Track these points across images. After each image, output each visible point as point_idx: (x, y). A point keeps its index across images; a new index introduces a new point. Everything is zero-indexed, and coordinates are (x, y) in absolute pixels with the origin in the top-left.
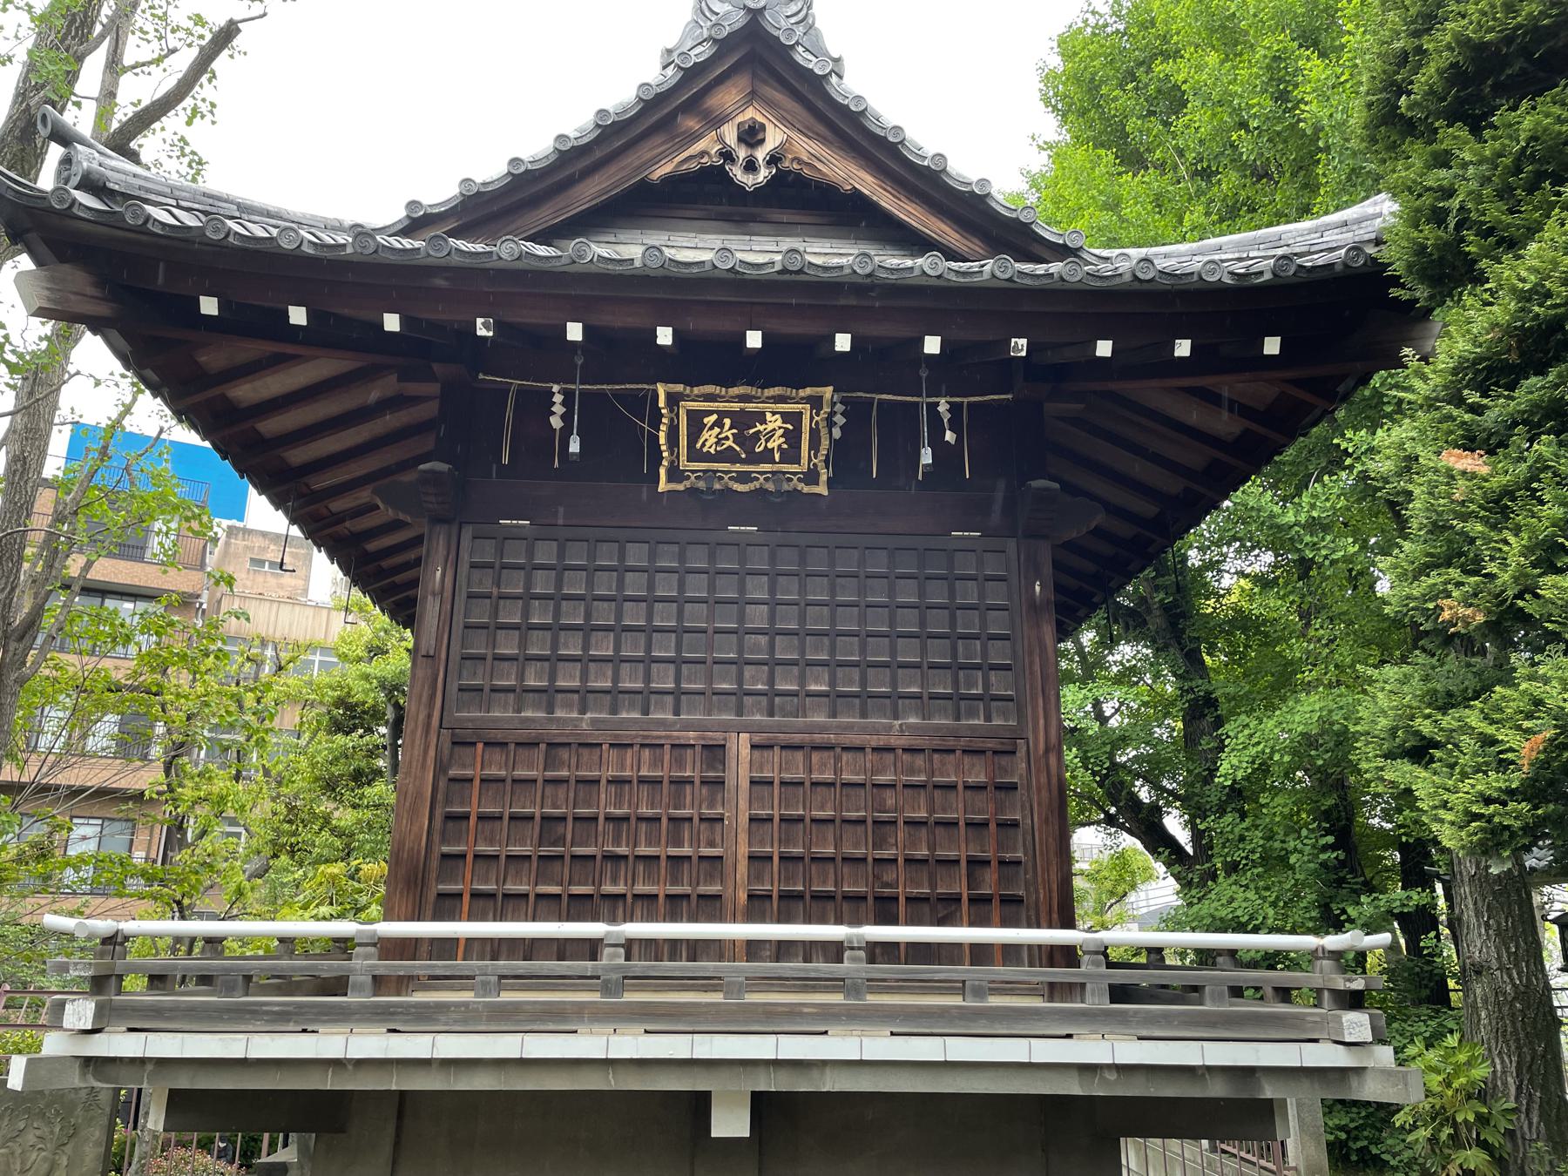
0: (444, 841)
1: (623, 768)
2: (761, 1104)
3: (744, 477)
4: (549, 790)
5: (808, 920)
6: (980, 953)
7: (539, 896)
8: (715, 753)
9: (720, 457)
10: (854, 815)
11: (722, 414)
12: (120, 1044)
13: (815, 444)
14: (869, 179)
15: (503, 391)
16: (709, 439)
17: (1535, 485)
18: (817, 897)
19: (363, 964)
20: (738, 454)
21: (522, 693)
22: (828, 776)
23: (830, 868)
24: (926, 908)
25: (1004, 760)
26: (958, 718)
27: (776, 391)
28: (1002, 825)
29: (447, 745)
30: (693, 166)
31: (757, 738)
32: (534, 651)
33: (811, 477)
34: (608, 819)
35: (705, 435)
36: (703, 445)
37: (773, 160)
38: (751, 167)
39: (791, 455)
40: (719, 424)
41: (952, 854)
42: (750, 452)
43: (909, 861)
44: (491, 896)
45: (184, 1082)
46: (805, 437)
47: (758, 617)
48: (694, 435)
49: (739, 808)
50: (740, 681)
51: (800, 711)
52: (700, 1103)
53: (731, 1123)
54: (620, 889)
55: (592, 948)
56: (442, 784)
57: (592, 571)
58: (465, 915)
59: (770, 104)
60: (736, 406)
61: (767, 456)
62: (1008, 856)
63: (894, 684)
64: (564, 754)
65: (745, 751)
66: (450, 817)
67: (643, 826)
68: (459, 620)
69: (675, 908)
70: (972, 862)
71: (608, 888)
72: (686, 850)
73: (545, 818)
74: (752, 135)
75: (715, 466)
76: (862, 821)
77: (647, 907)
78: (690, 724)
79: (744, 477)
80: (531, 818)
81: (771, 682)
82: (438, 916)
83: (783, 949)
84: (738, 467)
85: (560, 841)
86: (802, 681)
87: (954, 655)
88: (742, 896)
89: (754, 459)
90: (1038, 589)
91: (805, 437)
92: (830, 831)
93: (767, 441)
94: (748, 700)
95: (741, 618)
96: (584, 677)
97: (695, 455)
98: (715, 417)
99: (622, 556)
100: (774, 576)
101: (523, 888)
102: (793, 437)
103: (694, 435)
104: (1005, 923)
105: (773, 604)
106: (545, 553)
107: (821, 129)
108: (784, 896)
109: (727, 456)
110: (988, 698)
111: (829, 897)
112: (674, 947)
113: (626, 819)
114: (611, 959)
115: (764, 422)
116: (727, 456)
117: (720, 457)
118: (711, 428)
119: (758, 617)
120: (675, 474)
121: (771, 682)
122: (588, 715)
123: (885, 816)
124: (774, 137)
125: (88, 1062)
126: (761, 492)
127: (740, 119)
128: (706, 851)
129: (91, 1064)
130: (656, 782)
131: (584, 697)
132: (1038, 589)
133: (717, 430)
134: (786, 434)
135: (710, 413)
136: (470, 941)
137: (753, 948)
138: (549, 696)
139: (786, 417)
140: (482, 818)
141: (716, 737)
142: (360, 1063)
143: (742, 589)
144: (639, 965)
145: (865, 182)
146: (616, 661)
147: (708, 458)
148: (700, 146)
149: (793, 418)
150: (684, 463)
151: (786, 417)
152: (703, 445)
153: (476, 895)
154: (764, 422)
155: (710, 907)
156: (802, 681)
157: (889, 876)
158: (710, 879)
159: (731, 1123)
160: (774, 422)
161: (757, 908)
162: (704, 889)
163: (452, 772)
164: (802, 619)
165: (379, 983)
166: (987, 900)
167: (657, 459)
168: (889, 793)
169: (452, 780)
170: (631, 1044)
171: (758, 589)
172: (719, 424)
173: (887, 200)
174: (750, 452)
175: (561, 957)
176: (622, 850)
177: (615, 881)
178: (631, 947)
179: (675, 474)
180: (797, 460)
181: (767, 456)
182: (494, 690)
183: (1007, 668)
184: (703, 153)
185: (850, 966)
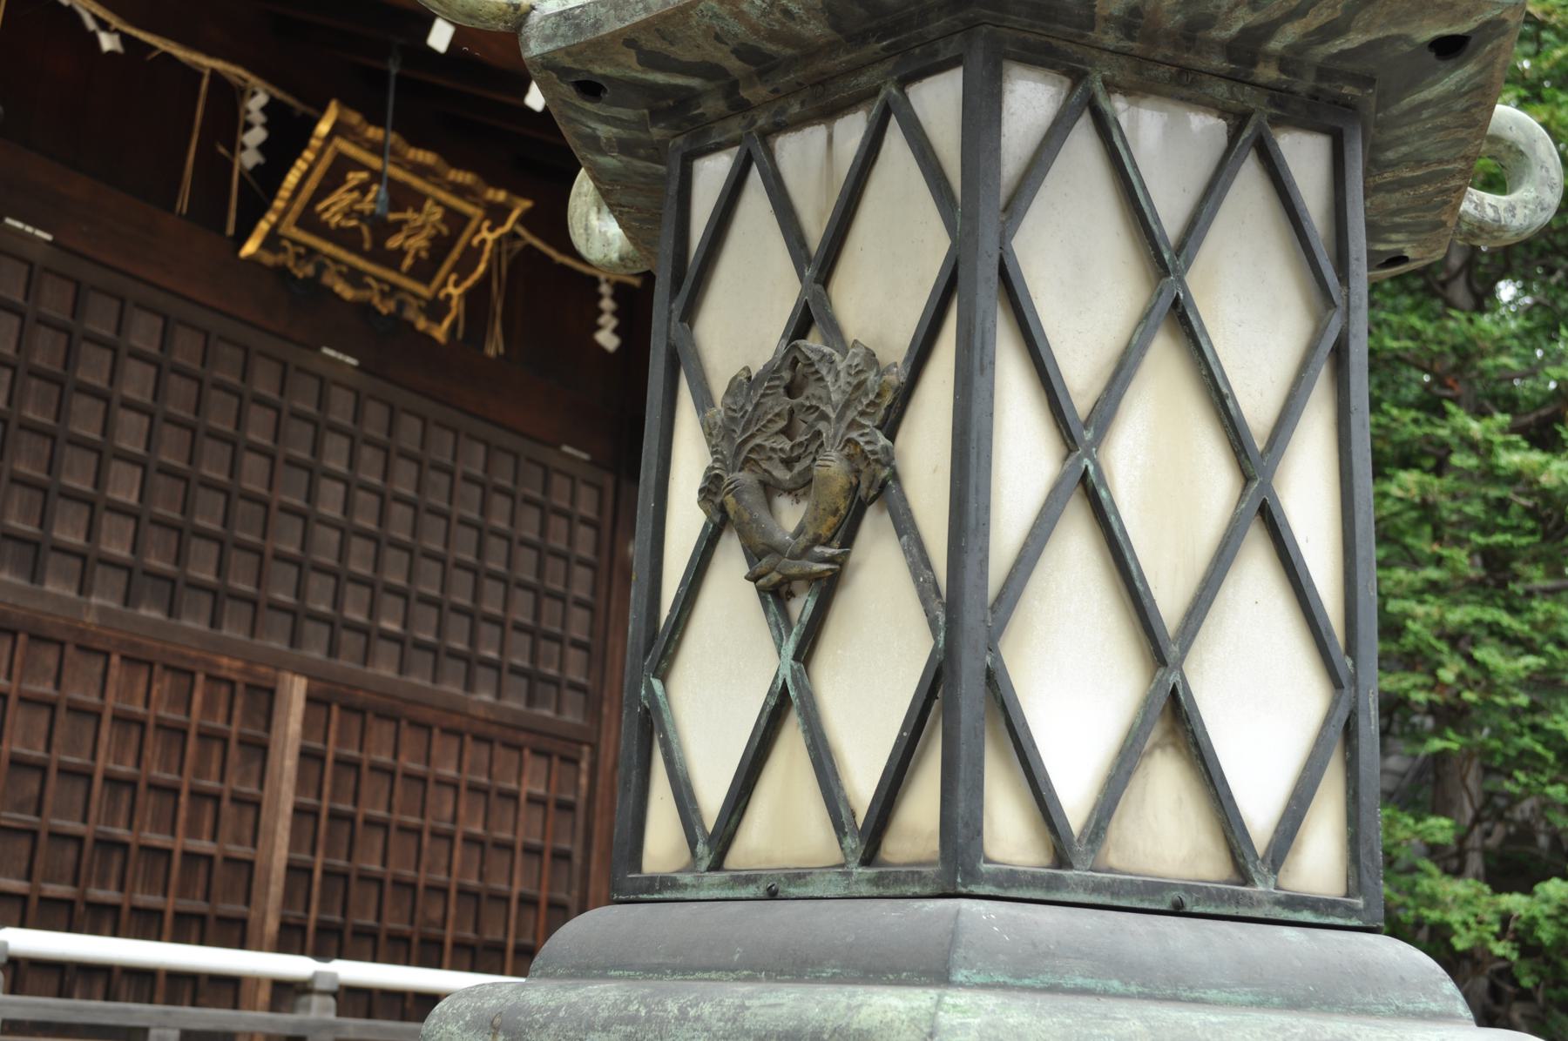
1: (131, 700)
3: (355, 277)
8: (265, 698)
11: (377, 176)
15: (193, 74)
17: (393, 243)
20: (362, 241)
36: (327, 209)
39: (424, 270)
40: (363, 188)
42: (379, 242)
46: (455, 254)
49: (284, 793)
58: (159, 995)
60: (400, 174)
61: (393, 259)
75: (328, 248)
79: (355, 277)
88: (272, 925)
93: (408, 237)
98: (363, 175)
102: (440, 246)
103: (323, 191)
115: (419, 209)
118: (351, 190)
122: (95, 600)
126: (365, 308)
133: (356, 195)
135: (359, 166)
149: (456, 220)
152: (327, 209)
154: (419, 209)
155: (237, 934)
172: (363, 188)
174: (379, 242)
175: (63, 992)
181: (393, 259)
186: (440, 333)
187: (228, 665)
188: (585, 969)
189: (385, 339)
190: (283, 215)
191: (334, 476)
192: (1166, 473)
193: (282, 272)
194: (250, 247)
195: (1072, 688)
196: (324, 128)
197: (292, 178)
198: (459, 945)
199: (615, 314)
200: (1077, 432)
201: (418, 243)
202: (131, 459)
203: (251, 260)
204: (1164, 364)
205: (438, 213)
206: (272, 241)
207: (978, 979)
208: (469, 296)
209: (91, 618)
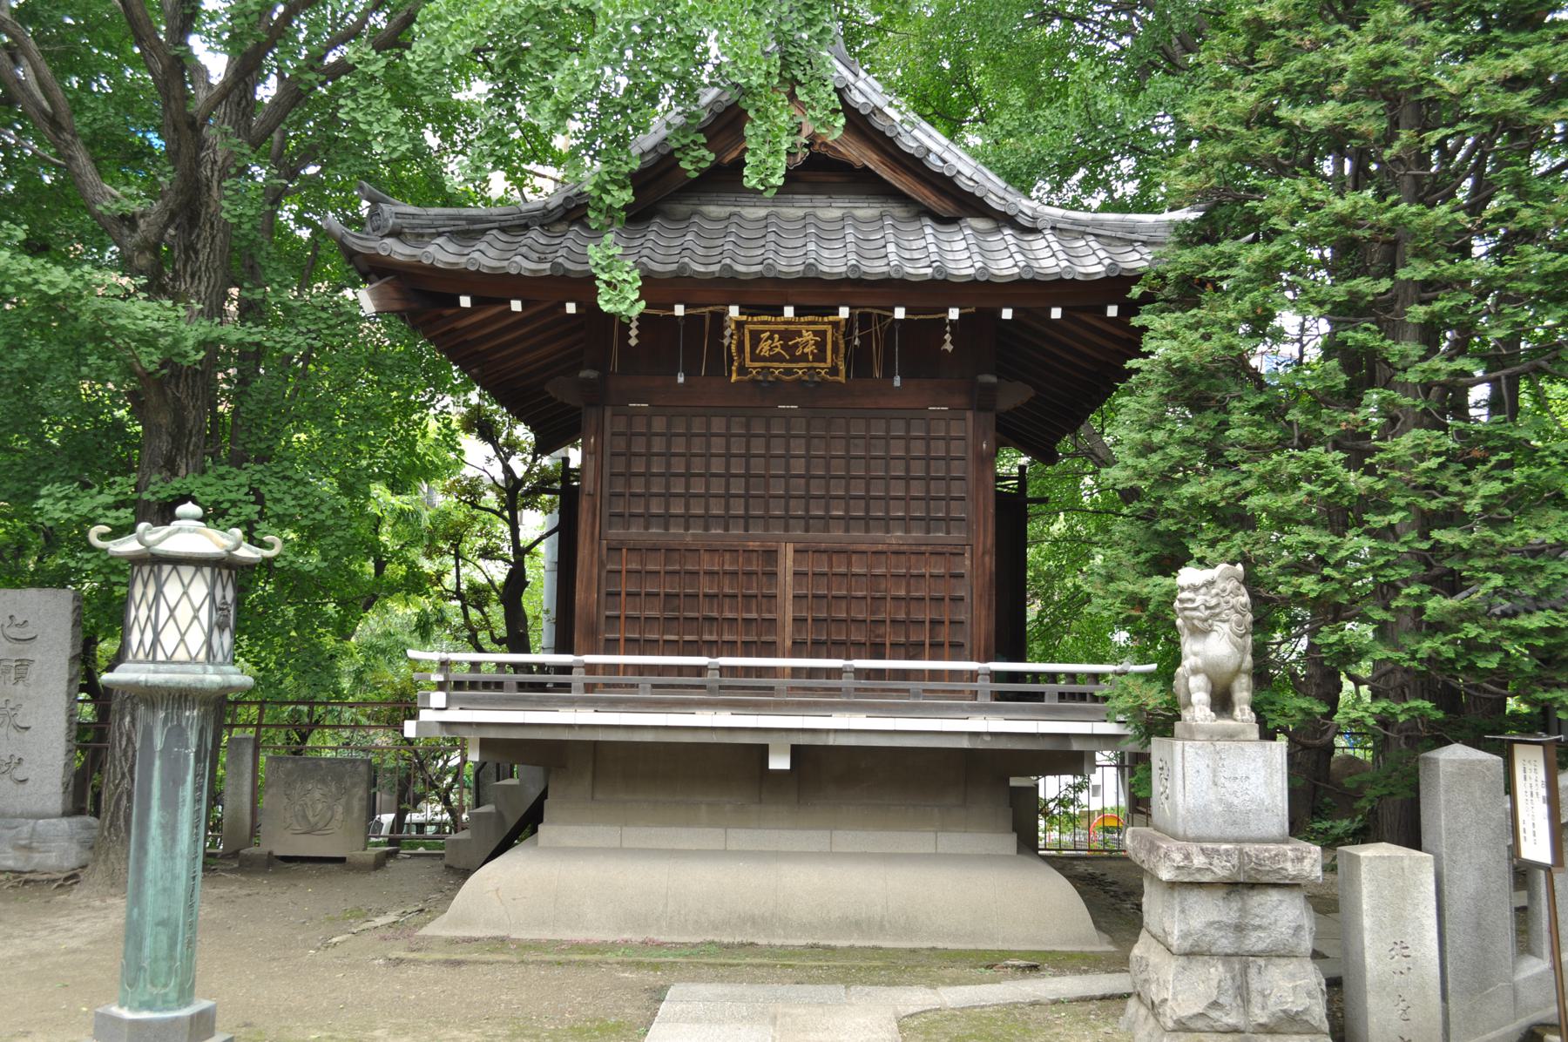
0: (607, 608)
2: (797, 752)
3: (789, 372)
4: (668, 578)
5: (829, 657)
6: (935, 675)
7: (665, 641)
8: (771, 555)
9: (773, 358)
10: (859, 594)
11: (773, 332)
12: (455, 715)
14: (875, 157)
16: (764, 348)
18: (835, 643)
19: (511, 677)
21: (648, 519)
22: (843, 570)
23: (844, 625)
24: (903, 650)
25: (957, 559)
26: (928, 532)
27: (810, 318)
28: (953, 599)
29: (604, 551)
31: (799, 546)
32: (654, 490)
33: (834, 370)
34: (705, 595)
35: (762, 344)
40: (771, 338)
41: (920, 617)
42: (792, 355)
43: (893, 621)
44: (637, 641)
45: (492, 734)
46: (829, 347)
47: (798, 467)
48: (754, 346)
49: (787, 585)
50: (787, 510)
51: (827, 529)
52: (762, 752)
53: (779, 762)
54: (714, 638)
55: (699, 671)
56: (604, 574)
57: (689, 436)
62: (957, 618)
63: (887, 511)
64: (676, 556)
65: (790, 554)
66: (609, 594)
67: (727, 600)
68: (606, 470)
69: (748, 649)
70: (932, 622)
71: (707, 637)
72: (754, 615)
73: (667, 595)
76: (865, 598)
77: (731, 649)
78: (756, 539)
80: (658, 595)
81: (807, 510)
82: (607, 652)
83: (812, 673)
84: (784, 365)
85: (678, 609)
86: (827, 509)
87: (928, 491)
88: (788, 643)
89: (794, 359)
91: (829, 347)
92: (844, 604)
94: (792, 521)
95: (787, 468)
96: (687, 507)
97: (755, 357)
99: (708, 426)
100: (809, 439)
101: (655, 637)
102: (821, 346)
103: (754, 346)
104: (932, 658)
105: (808, 458)
106: (659, 424)
108: (815, 643)
109: (777, 358)
110: (948, 520)
111: (843, 643)
112: (748, 671)
113: (716, 596)
114: (577, 678)
115: (801, 336)
116: (777, 358)
117: (773, 358)
119: (798, 467)
120: (742, 370)
121: (807, 510)
123: (878, 595)
125: (443, 724)
126: (799, 381)
128: (767, 616)
129: (446, 725)
130: (735, 573)
131: (687, 520)
134: (816, 343)
136: (626, 666)
137: (796, 672)
138: (666, 519)
140: (628, 594)
141: (771, 545)
142: (582, 726)
143: (788, 448)
144: (727, 681)
146: (706, 496)
147: (764, 359)
150: (748, 363)
151: (816, 333)
153: (627, 640)
154: (801, 336)
155: (769, 649)
156: (827, 509)
157: (881, 630)
158: (768, 633)
159: (779, 762)
160: (808, 336)
161: (798, 650)
162: (764, 638)
163: (610, 567)
164: (828, 468)
165: (589, 688)
166: (941, 645)
167: (731, 361)
168: (882, 580)
169: (610, 572)
170: (725, 719)
171: (798, 448)
172: (771, 338)
173: (886, 173)
174: (792, 355)
175: (680, 675)
176: (715, 614)
177: (711, 633)
178: (722, 670)
179: (742, 370)
180: (825, 361)
182: (632, 515)
183: (962, 499)
185: (847, 682)
186: (842, 378)
187: (752, 545)
188: (126, 671)
189: (811, 392)
192: (184, 613)
193: (754, 381)
194: (734, 378)
195: (169, 638)
200: (172, 611)
203: (737, 382)
204: (185, 599)
209: (689, 539)
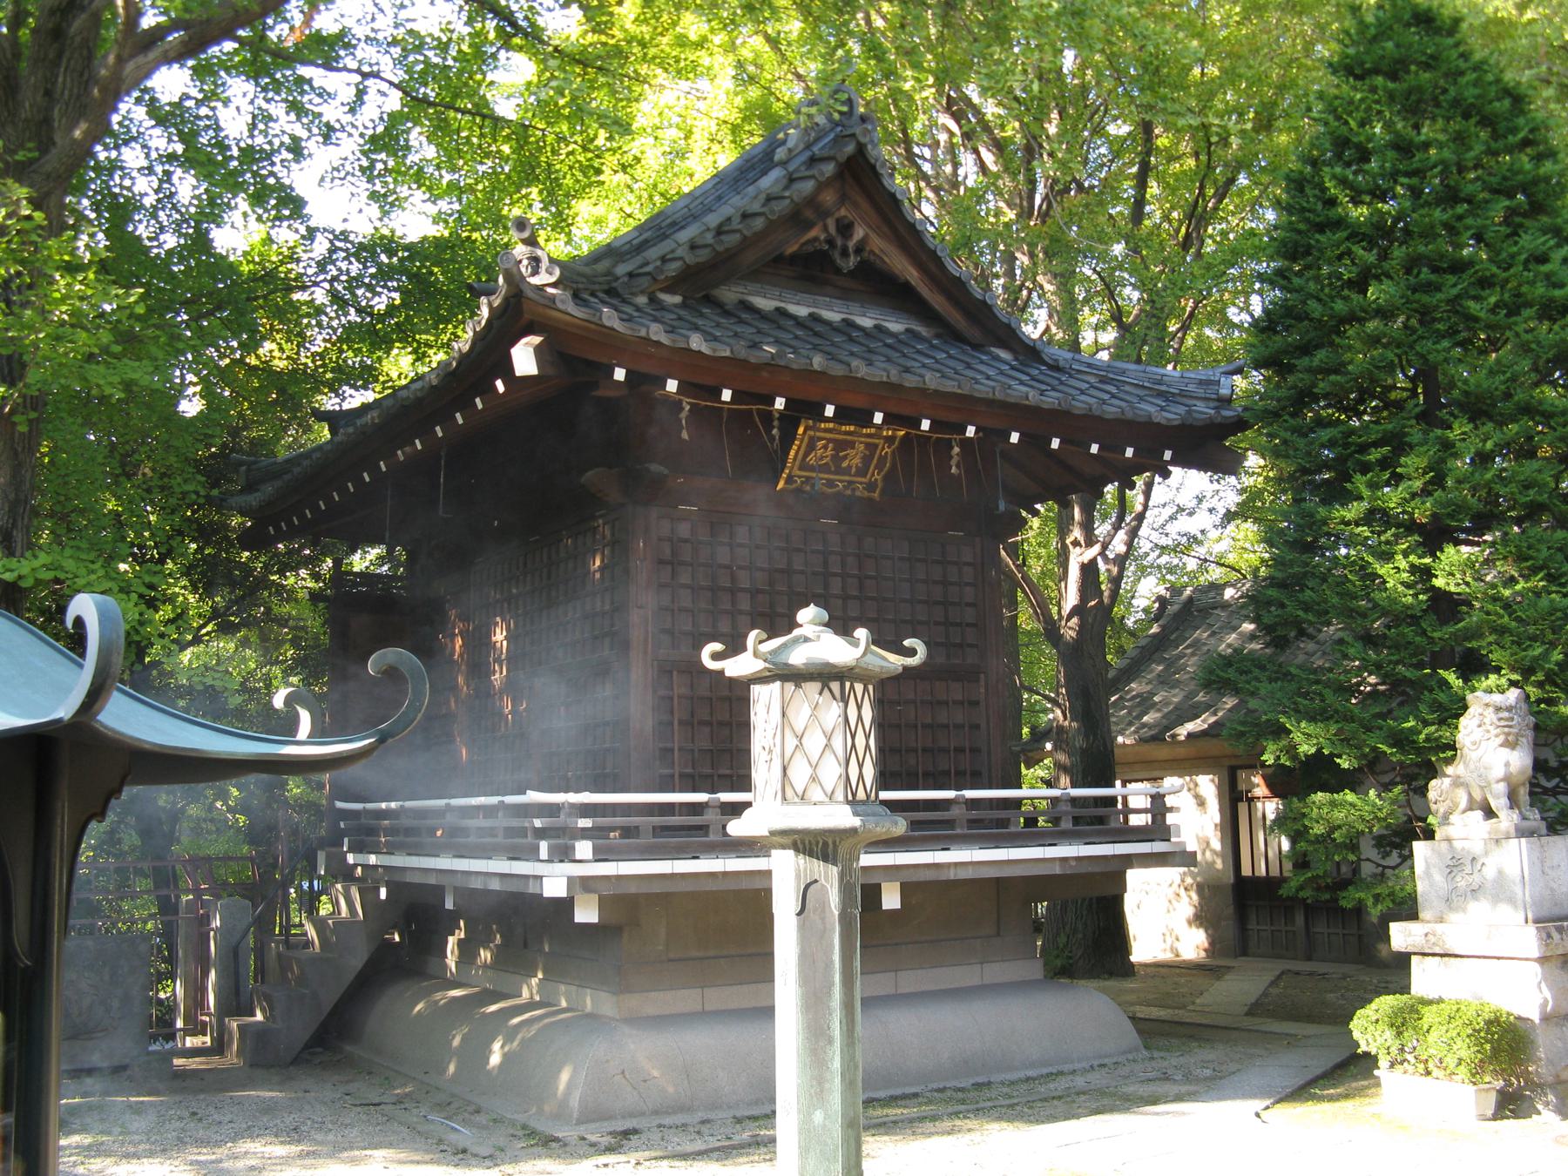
3: (830, 483)
11: (829, 441)
13: (880, 467)
14: (915, 273)
17: (845, 464)
30: (810, 249)
37: (859, 250)
38: (845, 253)
39: (862, 472)
59: (856, 205)
61: (847, 471)
74: (845, 228)
90: (452, 1068)
102: (867, 460)
103: (806, 454)
107: (886, 229)
109: (824, 468)
116: (824, 468)
124: (859, 233)
127: (837, 215)
132: (452, 1068)
136: (682, 804)
139: (868, 445)
145: (912, 275)
147: (812, 469)
148: (813, 233)
172: (825, 447)
173: (925, 291)
184: (816, 239)
190: (791, 469)
191: (835, 575)
194: (781, 485)
196: (801, 431)
197: (792, 453)
198: (926, 774)
199: (116, 110)
201: (857, 461)
202: (855, 597)
205: (862, 447)
206: (789, 480)
207: (699, 1145)
208: (885, 478)
